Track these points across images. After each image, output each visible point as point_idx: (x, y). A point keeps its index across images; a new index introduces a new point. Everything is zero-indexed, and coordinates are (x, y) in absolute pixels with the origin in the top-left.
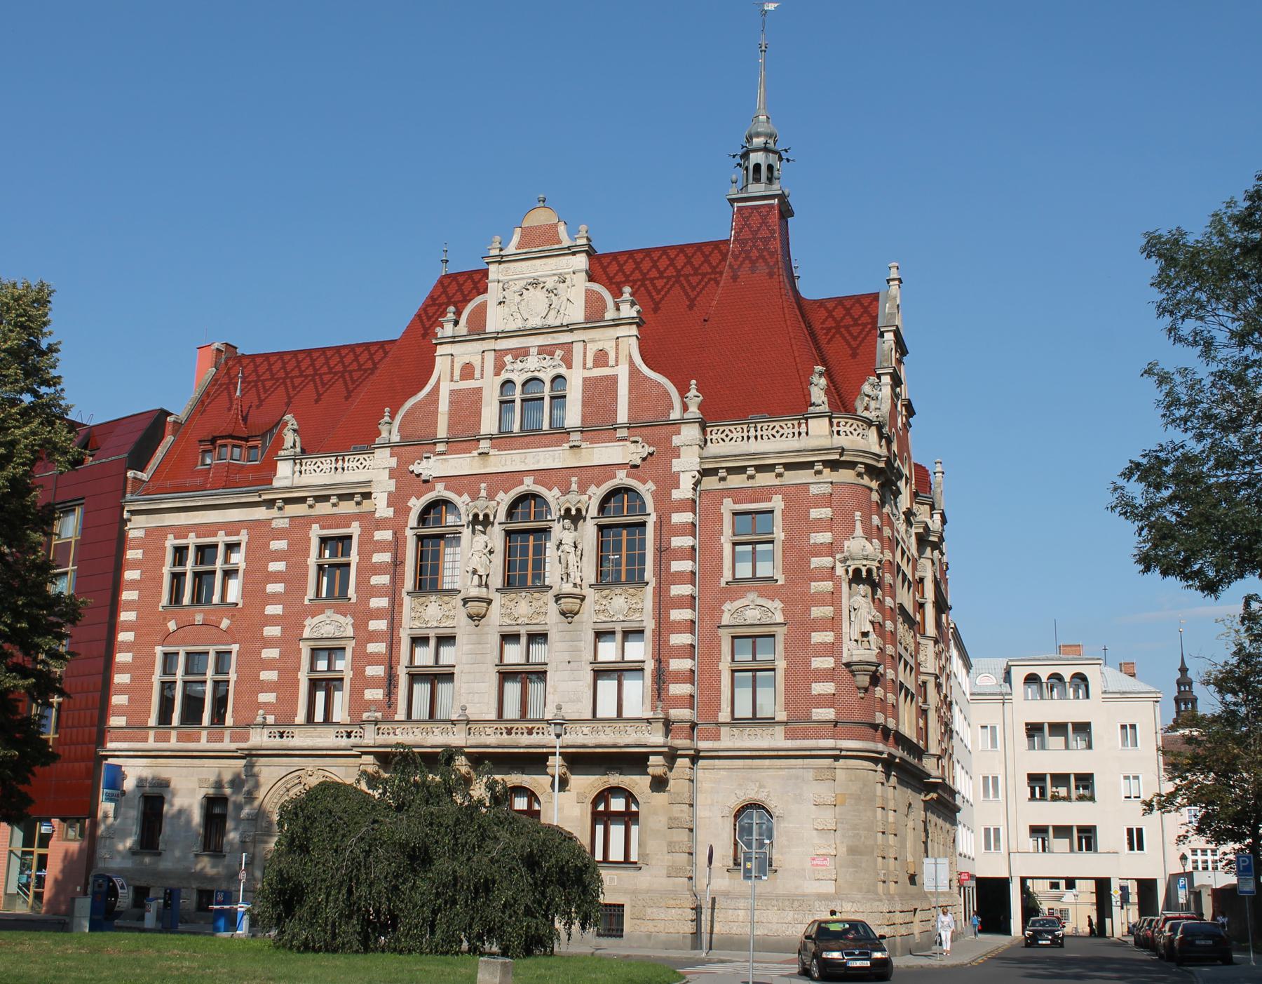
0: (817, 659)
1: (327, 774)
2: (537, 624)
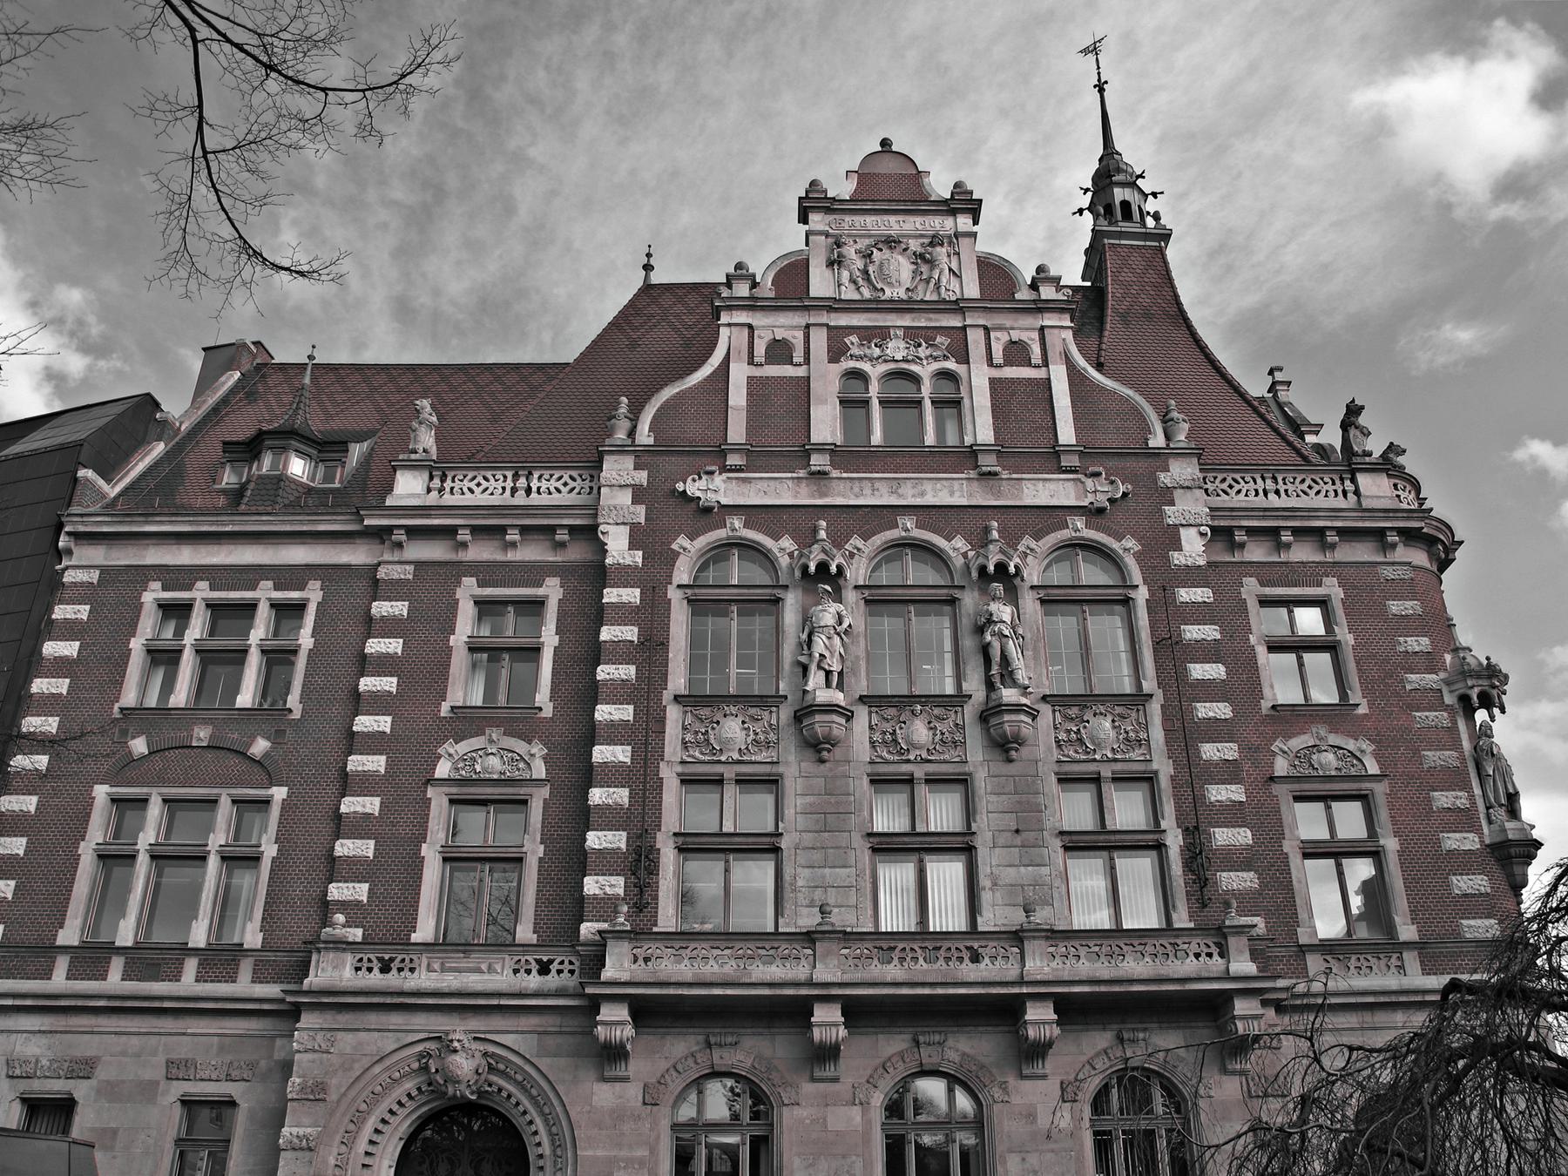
0: (1450, 835)
1: (491, 1049)
2: (945, 762)
